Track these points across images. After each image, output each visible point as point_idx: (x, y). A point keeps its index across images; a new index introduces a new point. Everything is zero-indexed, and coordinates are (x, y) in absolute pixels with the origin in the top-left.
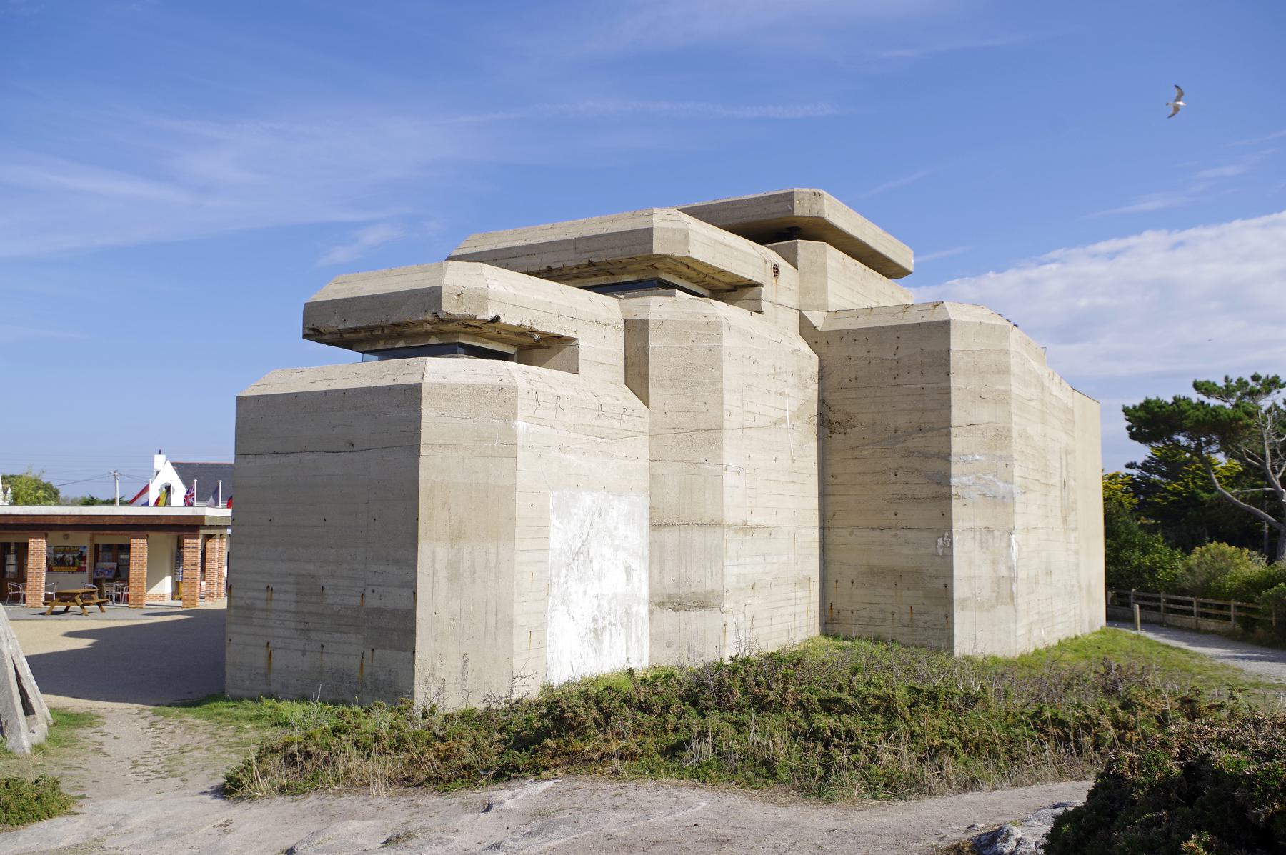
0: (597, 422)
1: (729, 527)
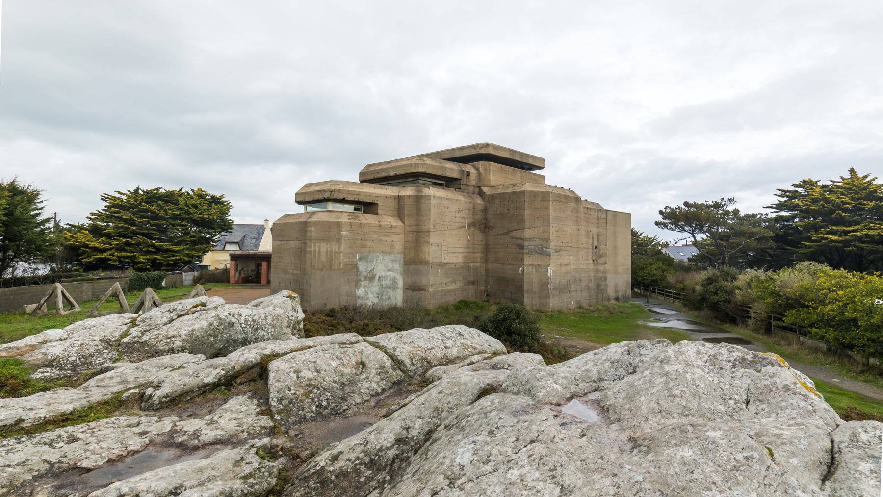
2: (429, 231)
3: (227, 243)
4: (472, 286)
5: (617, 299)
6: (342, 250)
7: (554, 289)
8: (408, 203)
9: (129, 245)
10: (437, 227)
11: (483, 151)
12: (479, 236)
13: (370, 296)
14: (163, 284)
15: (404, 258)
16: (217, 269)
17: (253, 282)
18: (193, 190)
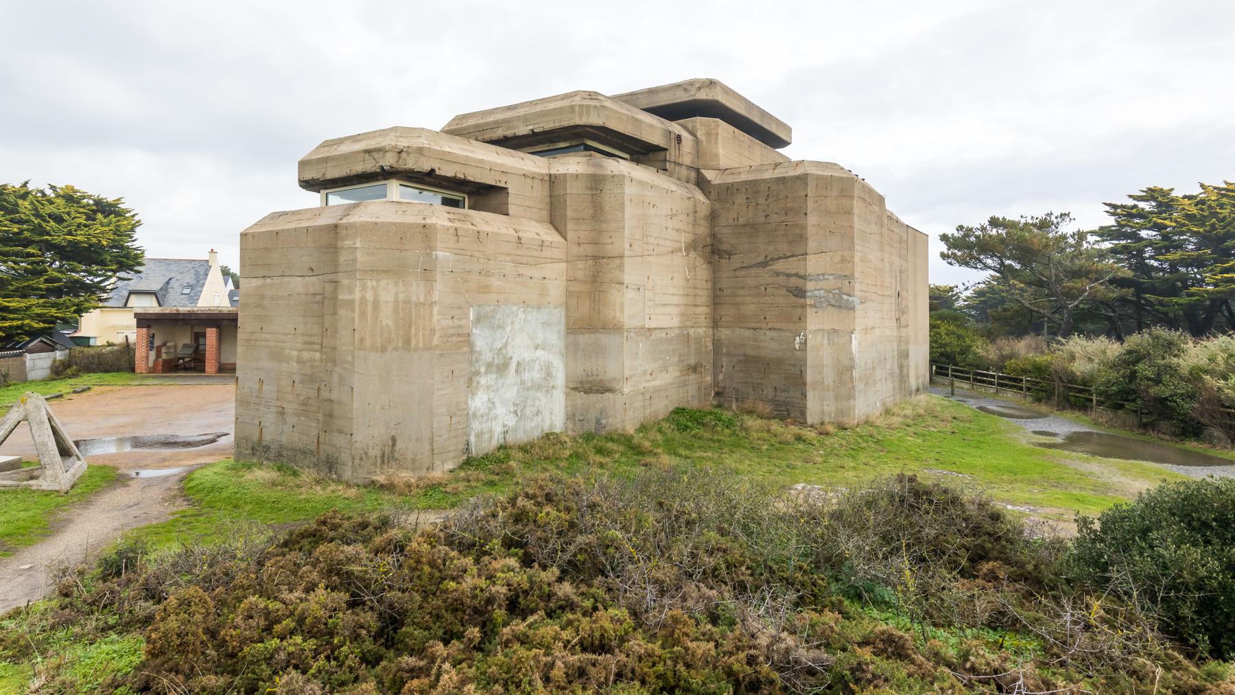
0: (519, 252)
1: (629, 330)
2: (621, 257)
3: (131, 293)
4: (693, 377)
6: (436, 296)
8: (574, 191)
10: (635, 247)
11: (703, 95)
12: (703, 272)
13: (500, 410)
15: (567, 316)
16: (110, 345)
17: (186, 369)
18: (53, 188)
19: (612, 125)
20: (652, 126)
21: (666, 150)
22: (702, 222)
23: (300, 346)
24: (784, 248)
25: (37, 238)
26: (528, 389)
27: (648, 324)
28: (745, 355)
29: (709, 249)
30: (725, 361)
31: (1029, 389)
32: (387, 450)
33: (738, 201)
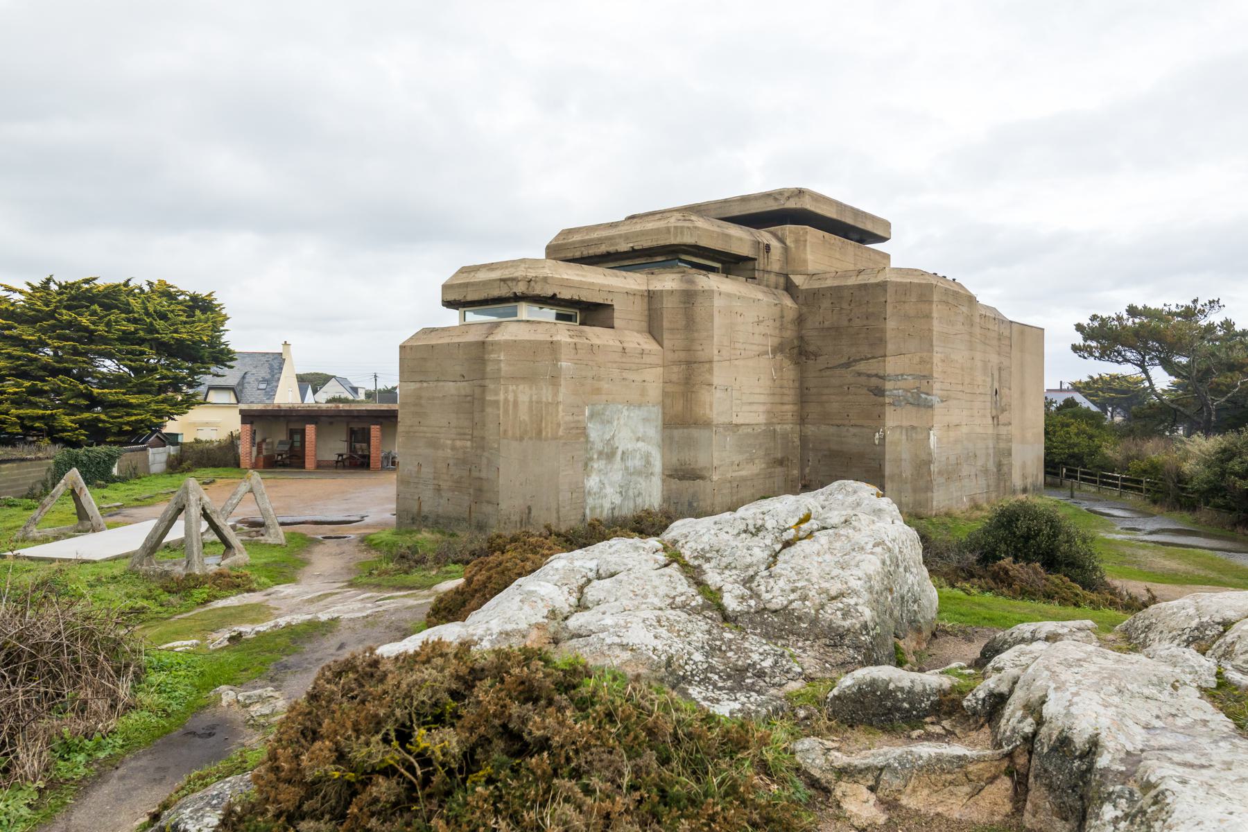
1: (717, 426)
2: (711, 362)
3: (211, 388)
4: (779, 470)
5: (1025, 490)
6: (561, 398)
7: (940, 473)
8: (669, 304)
9: (41, 393)
10: (724, 352)
11: (792, 204)
12: (790, 372)
13: (609, 490)
14: (115, 471)
15: (663, 413)
17: (284, 465)
18: (150, 284)
19: (704, 243)
20: (741, 239)
21: (755, 259)
22: (789, 326)
23: (453, 436)
24: (865, 350)
25: (148, 337)
26: (631, 474)
27: (736, 420)
28: (829, 450)
29: (796, 351)
30: (811, 456)
31: (1148, 490)
32: (525, 516)
33: (823, 306)
